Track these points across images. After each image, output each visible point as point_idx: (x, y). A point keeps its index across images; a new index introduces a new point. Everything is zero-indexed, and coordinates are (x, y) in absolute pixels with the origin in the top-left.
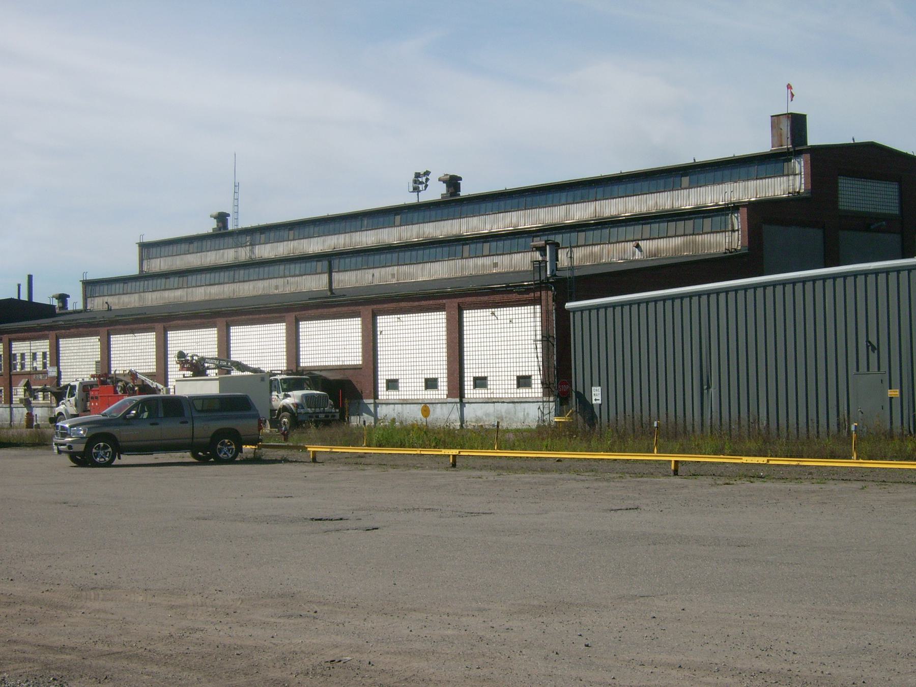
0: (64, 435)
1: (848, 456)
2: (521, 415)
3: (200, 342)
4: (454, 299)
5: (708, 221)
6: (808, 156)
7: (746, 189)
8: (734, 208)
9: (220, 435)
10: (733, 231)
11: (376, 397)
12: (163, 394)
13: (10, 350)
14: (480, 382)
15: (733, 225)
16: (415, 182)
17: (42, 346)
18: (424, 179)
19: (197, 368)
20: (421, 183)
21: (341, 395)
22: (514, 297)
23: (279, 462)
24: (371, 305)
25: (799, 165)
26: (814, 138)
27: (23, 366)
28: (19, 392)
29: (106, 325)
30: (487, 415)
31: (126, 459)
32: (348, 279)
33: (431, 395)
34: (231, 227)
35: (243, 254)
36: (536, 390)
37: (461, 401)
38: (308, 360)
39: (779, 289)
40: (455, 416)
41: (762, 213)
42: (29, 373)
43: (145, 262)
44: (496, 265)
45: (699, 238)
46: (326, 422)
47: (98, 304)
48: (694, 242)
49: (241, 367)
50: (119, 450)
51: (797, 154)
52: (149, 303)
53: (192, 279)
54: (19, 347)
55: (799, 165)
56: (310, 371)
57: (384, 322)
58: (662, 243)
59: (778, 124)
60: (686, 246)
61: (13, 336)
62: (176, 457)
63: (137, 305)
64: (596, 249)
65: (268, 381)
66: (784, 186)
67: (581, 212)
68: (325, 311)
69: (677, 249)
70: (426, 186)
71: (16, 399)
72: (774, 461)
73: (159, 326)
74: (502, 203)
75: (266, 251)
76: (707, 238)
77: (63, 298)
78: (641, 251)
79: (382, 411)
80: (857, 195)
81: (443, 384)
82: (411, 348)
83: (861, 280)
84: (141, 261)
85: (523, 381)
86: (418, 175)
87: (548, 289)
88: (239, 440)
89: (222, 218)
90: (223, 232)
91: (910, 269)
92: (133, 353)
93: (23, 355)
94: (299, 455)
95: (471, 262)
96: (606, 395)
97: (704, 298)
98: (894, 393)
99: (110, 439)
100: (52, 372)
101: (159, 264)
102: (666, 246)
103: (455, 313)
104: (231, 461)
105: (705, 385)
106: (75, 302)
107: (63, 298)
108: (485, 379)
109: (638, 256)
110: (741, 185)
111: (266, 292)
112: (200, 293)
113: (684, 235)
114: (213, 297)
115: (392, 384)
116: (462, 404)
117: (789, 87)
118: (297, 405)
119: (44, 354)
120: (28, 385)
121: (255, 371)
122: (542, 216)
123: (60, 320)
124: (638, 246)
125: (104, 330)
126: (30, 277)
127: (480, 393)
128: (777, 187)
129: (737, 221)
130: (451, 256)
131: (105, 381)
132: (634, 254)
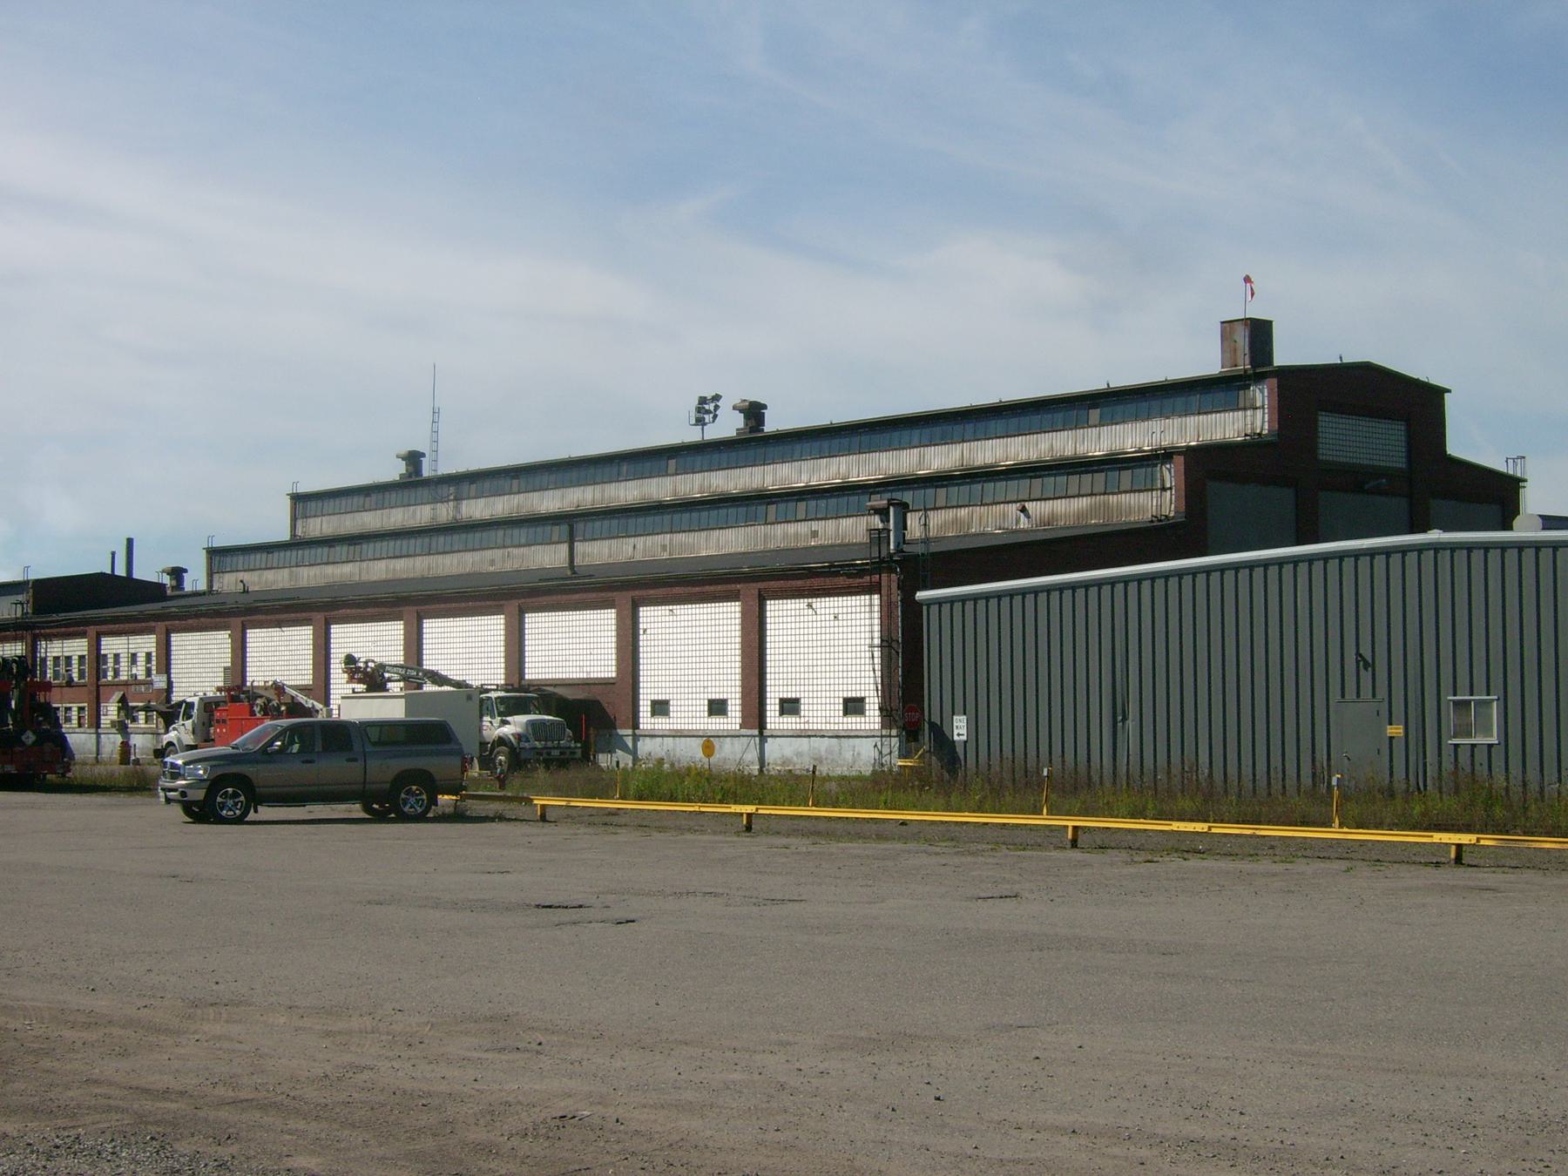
3: (379, 642)
4: (755, 584)
6: (1274, 381)
10: (1164, 489)
11: (636, 726)
13: (98, 649)
14: (790, 706)
15: (1163, 481)
16: (699, 410)
17: (146, 644)
18: (711, 407)
19: (373, 679)
20: (708, 412)
21: (584, 724)
22: (841, 581)
24: (629, 591)
25: (1261, 394)
26: (1284, 355)
27: (116, 673)
28: (111, 711)
29: (240, 615)
30: (799, 754)
31: (265, 812)
32: (597, 552)
33: (716, 724)
35: (444, 513)
36: (872, 719)
37: (761, 733)
38: (533, 672)
40: (752, 755)
41: (1205, 463)
42: (126, 684)
43: (299, 523)
44: (815, 534)
45: (1113, 499)
47: (228, 583)
48: (1106, 505)
50: (256, 798)
51: (1259, 378)
52: (304, 583)
53: (368, 548)
54: (112, 645)
55: (1261, 394)
56: (538, 686)
57: (648, 615)
58: (1060, 506)
59: (1232, 332)
60: (1093, 510)
61: (104, 628)
63: (287, 586)
64: (963, 512)
65: (475, 699)
67: (940, 458)
69: (1080, 515)
70: (715, 417)
71: (105, 721)
72: (1219, 829)
75: (477, 508)
76: (1124, 498)
77: (177, 573)
78: (1028, 517)
79: (645, 747)
81: (735, 708)
82: (687, 658)
84: (294, 519)
85: (853, 706)
86: (703, 400)
87: (891, 570)
88: (433, 787)
89: (414, 459)
90: (415, 480)
92: (280, 656)
93: (117, 656)
96: (974, 727)
98: (1396, 730)
99: (243, 782)
100: (160, 682)
101: (319, 526)
102: (1065, 510)
103: (628, 612)
104: (421, 818)
105: (1119, 715)
106: (196, 580)
108: (796, 701)
109: (1024, 523)
110: (1176, 421)
111: (477, 569)
112: (379, 569)
113: (1092, 494)
114: (398, 576)
115: (660, 708)
116: (763, 738)
117: (1247, 280)
118: (519, 737)
119: (149, 655)
120: (123, 700)
121: (459, 684)
122: (884, 463)
124: (1023, 510)
125: (237, 621)
126: (130, 542)
127: (790, 723)
129: (1170, 475)
130: (750, 521)
132: (1018, 521)
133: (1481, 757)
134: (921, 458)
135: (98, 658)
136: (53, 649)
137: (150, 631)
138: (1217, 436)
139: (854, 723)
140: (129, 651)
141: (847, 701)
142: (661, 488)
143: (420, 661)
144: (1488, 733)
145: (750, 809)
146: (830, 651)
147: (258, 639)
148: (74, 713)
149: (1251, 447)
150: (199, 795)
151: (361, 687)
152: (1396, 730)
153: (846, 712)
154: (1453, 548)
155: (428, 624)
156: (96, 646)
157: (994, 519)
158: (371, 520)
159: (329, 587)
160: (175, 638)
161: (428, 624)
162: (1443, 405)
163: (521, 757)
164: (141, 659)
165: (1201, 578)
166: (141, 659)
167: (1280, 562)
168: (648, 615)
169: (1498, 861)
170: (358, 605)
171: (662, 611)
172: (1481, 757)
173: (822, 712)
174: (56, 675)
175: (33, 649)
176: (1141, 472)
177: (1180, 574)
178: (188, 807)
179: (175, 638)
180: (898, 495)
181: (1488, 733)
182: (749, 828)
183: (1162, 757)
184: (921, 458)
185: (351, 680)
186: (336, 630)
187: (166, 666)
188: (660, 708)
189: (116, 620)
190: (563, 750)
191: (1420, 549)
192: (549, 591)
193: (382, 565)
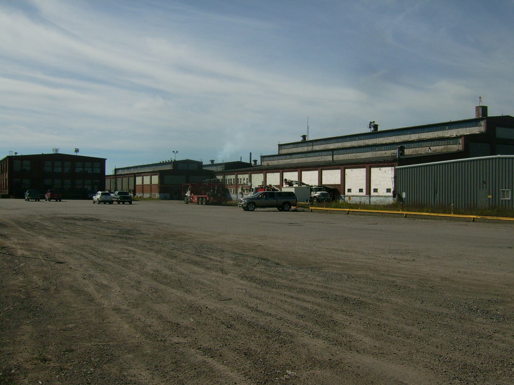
0: (241, 202)
1: (450, 213)
2: (387, 201)
3: (291, 176)
4: (369, 165)
5: (452, 141)
6: (485, 120)
7: (466, 130)
8: (457, 137)
9: (285, 203)
11: (344, 194)
12: (279, 191)
14: (376, 190)
17: (246, 176)
19: (290, 184)
21: (333, 194)
23: (301, 211)
24: (343, 166)
25: (483, 123)
26: (490, 114)
28: (240, 190)
29: (265, 170)
31: (258, 209)
32: (340, 157)
33: (361, 194)
34: (379, 130)
35: (310, 148)
36: (391, 194)
38: (324, 182)
39: (469, 162)
40: (368, 201)
41: (468, 138)
42: (242, 185)
44: (386, 153)
45: (449, 146)
46: (329, 201)
47: (265, 163)
49: (304, 184)
50: (256, 206)
51: (482, 119)
52: (280, 164)
53: (294, 156)
54: (240, 176)
55: (483, 123)
56: (325, 186)
57: (347, 171)
60: (445, 148)
62: (271, 209)
64: (417, 149)
65: (311, 189)
66: (436, 134)
67: (414, 137)
68: (330, 167)
69: (441, 150)
71: (238, 192)
72: (431, 214)
73: (281, 171)
74: (390, 134)
75: (317, 148)
77: (255, 161)
79: (347, 199)
80: (501, 133)
81: (364, 191)
82: (355, 179)
83: (481, 161)
84: (279, 150)
85: (388, 190)
86: (371, 123)
87: (396, 162)
88: (290, 205)
89: (304, 137)
90: (305, 141)
91: (512, 158)
92: (273, 179)
94: (306, 209)
95: (378, 152)
96: (407, 195)
97: (436, 166)
98: (490, 197)
99: (254, 203)
100: (249, 184)
101: (284, 151)
102: (439, 148)
103: (343, 170)
104: (288, 211)
105: (435, 192)
106: (259, 163)
107: (255, 161)
108: (377, 189)
109: (430, 151)
110: (464, 129)
112: (295, 161)
115: (349, 190)
116: (370, 197)
117: (480, 98)
118: (319, 196)
120: (242, 188)
121: (307, 185)
123: (252, 168)
125: (265, 172)
126: (251, 153)
127: (375, 194)
128: (475, 130)
129: (461, 141)
130: (373, 150)
131: (264, 186)
133: (507, 202)
134: (410, 137)
135: (237, 179)
136: (228, 177)
137: (247, 173)
138: (473, 132)
139: (361, 194)
140: (243, 177)
141: (387, 189)
142: (355, 143)
143: (301, 181)
144: (509, 197)
145: (348, 210)
146: (384, 179)
147: (269, 175)
148: (232, 191)
149: (481, 134)
150: (246, 206)
151: (288, 185)
152: (490, 197)
153: (387, 192)
154: (502, 158)
155: (303, 172)
156: (237, 177)
157: (423, 150)
158: (295, 150)
159: (285, 164)
160: (252, 175)
161: (303, 172)
162: (105, 182)
163: (319, 201)
164: (246, 179)
165: (463, 163)
166: (246, 179)
167: (486, 159)
168: (347, 171)
169: (479, 221)
170: (288, 168)
171: (350, 170)
172: (507, 202)
173: (382, 192)
174: (229, 183)
175: (224, 177)
176: (455, 140)
177: (465, 161)
178: (244, 208)
179: (252, 175)
180: (403, 145)
181: (509, 197)
182: (348, 213)
183: (428, 200)
184: (410, 137)
185: (286, 184)
186: (284, 173)
187: (251, 181)
188: (349, 190)
189: (242, 171)
190: (328, 199)
191: (496, 158)
192: (327, 166)
193: (282, 161)
